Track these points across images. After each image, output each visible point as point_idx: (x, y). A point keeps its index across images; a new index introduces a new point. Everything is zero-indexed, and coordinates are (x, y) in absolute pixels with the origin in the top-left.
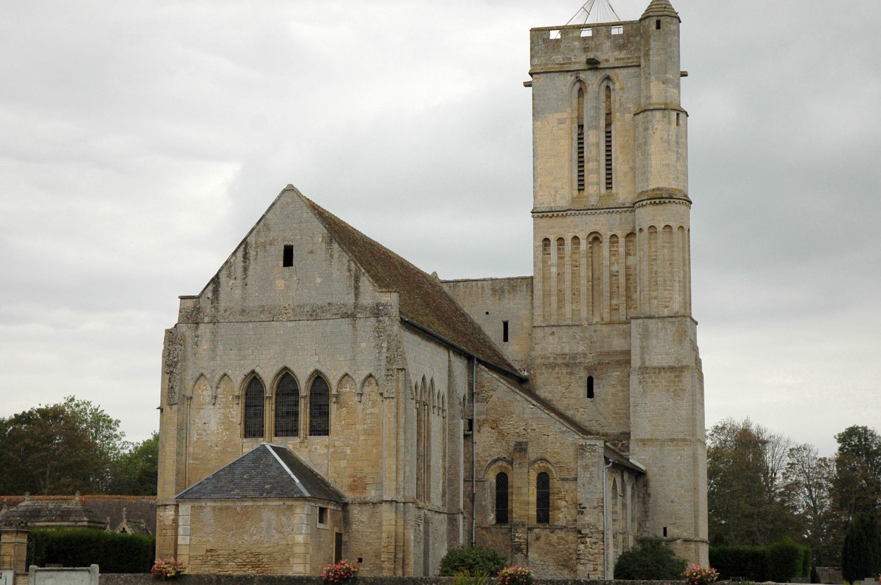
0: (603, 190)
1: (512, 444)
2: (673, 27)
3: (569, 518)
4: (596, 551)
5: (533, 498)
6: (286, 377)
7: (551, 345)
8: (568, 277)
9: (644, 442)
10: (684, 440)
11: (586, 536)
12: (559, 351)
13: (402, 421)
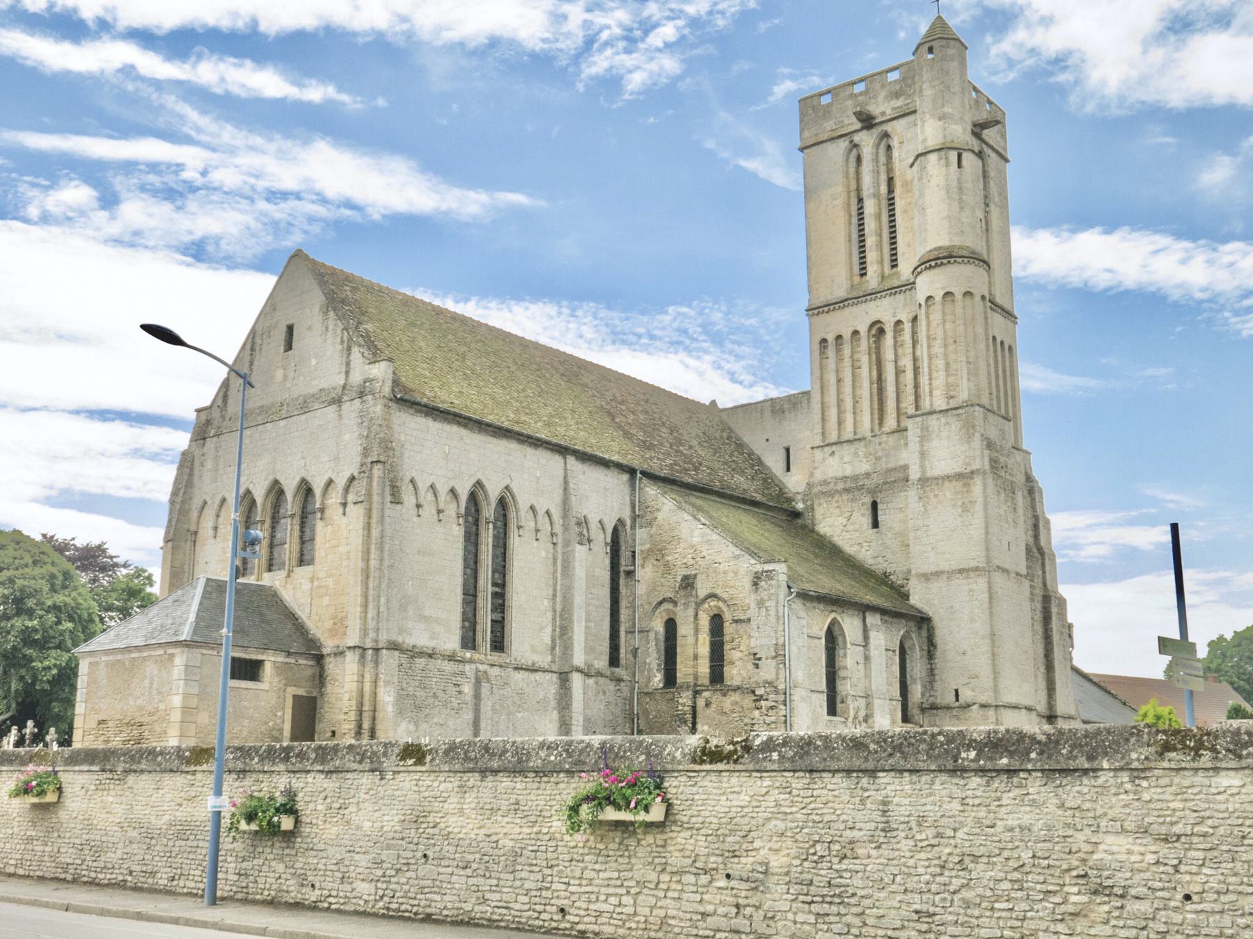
1: (679, 579)
4: (773, 719)
9: (926, 577)
10: (977, 569)
11: (760, 698)
13: (375, 533)
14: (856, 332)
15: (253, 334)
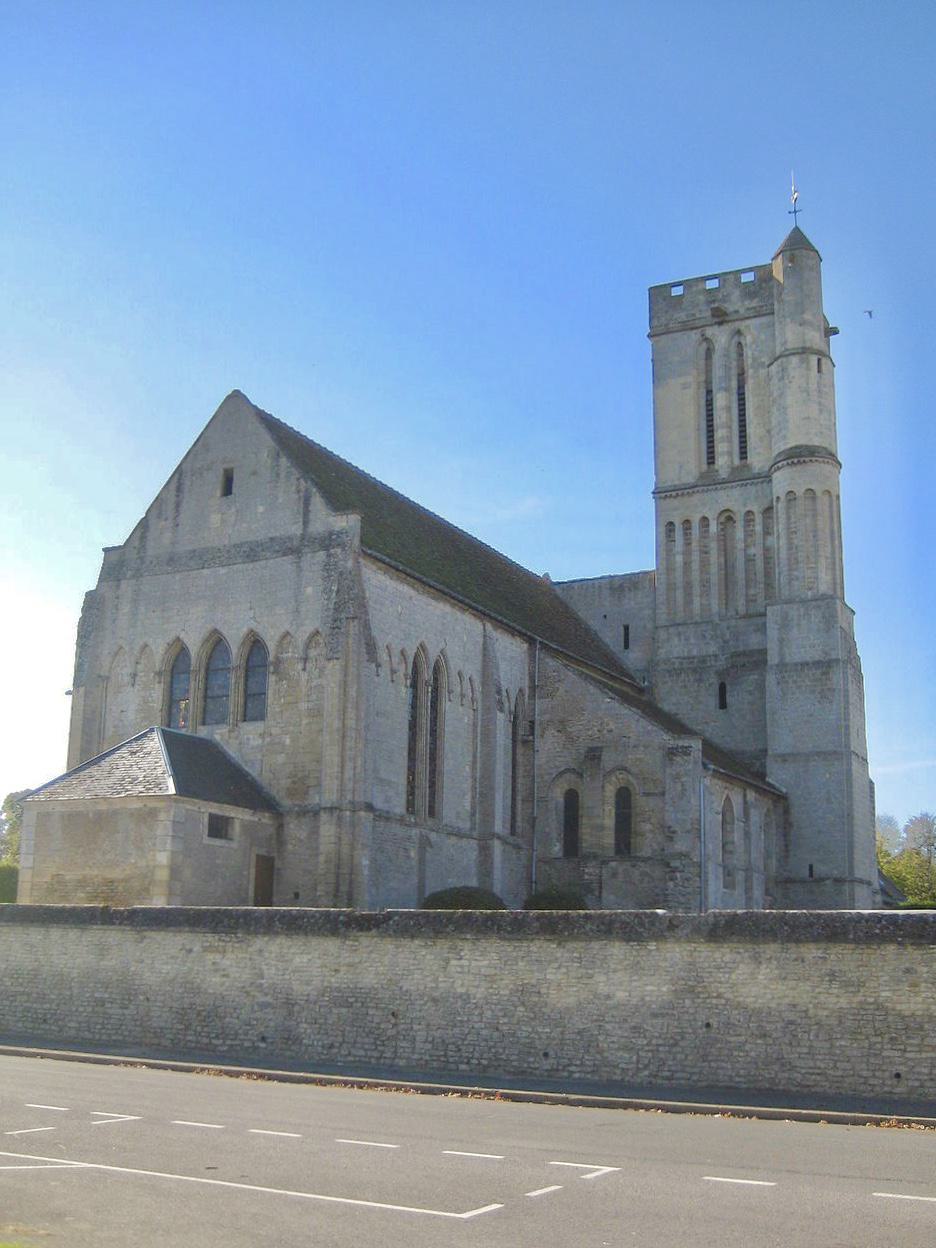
0: (737, 462)
2: (811, 262)
3: (655, 846)
4: (688, 890)
5: (610, 821)
6: (217, 643)
7: (675, 648)
8: (695, 566)
9: (784, 758)
11: (674, 870)
12: (686, 654)
13: (353, 692)
14: (705, 519)
15: (179, 471)
